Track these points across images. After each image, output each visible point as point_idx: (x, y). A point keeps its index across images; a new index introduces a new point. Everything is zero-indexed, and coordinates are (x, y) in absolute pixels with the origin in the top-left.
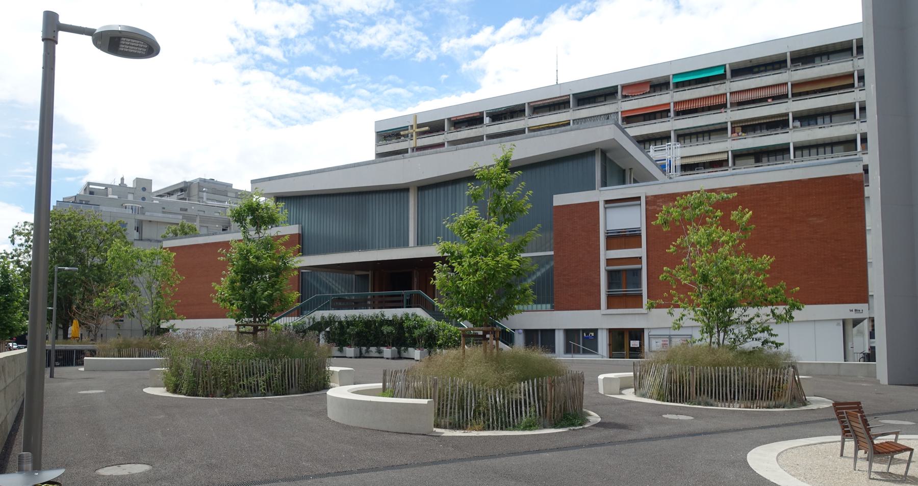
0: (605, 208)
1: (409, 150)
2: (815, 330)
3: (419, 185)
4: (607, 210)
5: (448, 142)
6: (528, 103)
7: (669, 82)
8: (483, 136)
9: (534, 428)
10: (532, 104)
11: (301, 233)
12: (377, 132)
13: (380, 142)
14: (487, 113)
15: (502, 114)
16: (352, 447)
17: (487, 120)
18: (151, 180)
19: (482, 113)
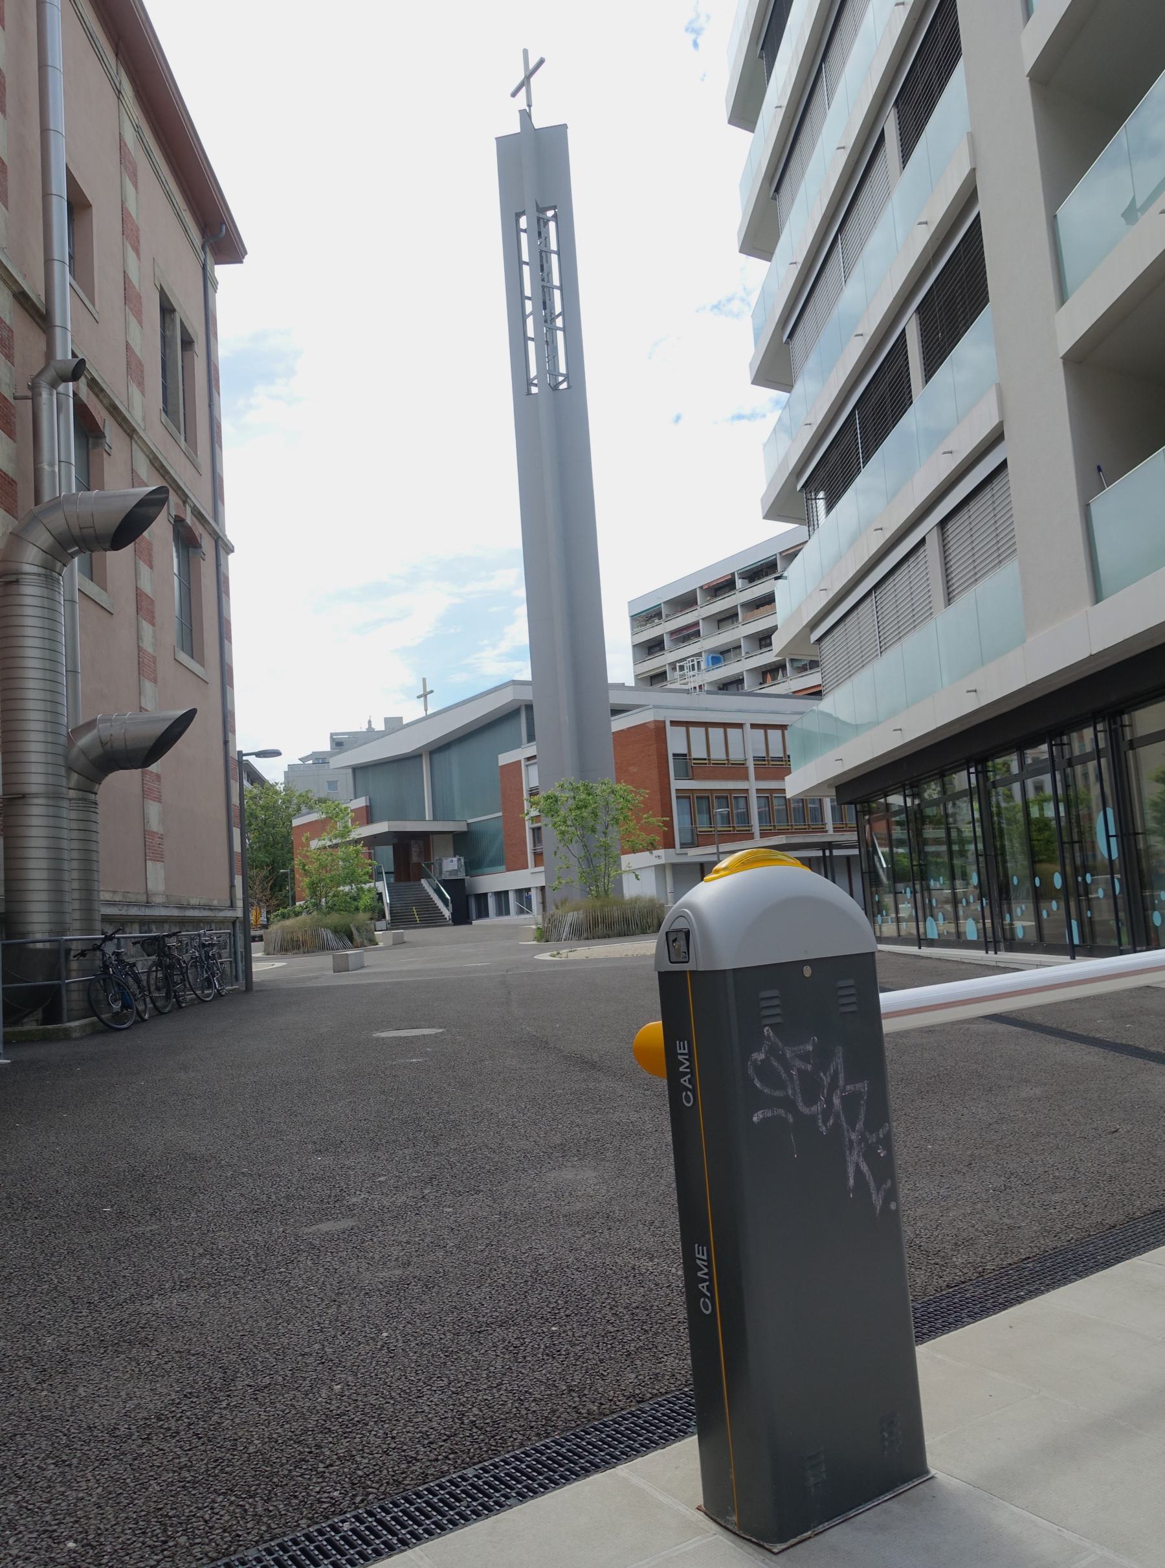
0: (527, 766)
1: (666, 639)
2: (7, 616)
3: (430, 750)
4: (529, 767)
5: (703, 619)
6: (780, 553)
7: (661, 612)
8: (737, 606)
9: (297, 951)
10: (784, 554)
11: (368, 804)
12: (632, 616)
13: (635, 630)
14: (739, 574)
15: (762, 570)
16: (155, 1227)
17: (739, 583)
18: (402, 718)
19: (733, 574)
